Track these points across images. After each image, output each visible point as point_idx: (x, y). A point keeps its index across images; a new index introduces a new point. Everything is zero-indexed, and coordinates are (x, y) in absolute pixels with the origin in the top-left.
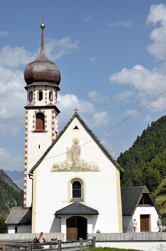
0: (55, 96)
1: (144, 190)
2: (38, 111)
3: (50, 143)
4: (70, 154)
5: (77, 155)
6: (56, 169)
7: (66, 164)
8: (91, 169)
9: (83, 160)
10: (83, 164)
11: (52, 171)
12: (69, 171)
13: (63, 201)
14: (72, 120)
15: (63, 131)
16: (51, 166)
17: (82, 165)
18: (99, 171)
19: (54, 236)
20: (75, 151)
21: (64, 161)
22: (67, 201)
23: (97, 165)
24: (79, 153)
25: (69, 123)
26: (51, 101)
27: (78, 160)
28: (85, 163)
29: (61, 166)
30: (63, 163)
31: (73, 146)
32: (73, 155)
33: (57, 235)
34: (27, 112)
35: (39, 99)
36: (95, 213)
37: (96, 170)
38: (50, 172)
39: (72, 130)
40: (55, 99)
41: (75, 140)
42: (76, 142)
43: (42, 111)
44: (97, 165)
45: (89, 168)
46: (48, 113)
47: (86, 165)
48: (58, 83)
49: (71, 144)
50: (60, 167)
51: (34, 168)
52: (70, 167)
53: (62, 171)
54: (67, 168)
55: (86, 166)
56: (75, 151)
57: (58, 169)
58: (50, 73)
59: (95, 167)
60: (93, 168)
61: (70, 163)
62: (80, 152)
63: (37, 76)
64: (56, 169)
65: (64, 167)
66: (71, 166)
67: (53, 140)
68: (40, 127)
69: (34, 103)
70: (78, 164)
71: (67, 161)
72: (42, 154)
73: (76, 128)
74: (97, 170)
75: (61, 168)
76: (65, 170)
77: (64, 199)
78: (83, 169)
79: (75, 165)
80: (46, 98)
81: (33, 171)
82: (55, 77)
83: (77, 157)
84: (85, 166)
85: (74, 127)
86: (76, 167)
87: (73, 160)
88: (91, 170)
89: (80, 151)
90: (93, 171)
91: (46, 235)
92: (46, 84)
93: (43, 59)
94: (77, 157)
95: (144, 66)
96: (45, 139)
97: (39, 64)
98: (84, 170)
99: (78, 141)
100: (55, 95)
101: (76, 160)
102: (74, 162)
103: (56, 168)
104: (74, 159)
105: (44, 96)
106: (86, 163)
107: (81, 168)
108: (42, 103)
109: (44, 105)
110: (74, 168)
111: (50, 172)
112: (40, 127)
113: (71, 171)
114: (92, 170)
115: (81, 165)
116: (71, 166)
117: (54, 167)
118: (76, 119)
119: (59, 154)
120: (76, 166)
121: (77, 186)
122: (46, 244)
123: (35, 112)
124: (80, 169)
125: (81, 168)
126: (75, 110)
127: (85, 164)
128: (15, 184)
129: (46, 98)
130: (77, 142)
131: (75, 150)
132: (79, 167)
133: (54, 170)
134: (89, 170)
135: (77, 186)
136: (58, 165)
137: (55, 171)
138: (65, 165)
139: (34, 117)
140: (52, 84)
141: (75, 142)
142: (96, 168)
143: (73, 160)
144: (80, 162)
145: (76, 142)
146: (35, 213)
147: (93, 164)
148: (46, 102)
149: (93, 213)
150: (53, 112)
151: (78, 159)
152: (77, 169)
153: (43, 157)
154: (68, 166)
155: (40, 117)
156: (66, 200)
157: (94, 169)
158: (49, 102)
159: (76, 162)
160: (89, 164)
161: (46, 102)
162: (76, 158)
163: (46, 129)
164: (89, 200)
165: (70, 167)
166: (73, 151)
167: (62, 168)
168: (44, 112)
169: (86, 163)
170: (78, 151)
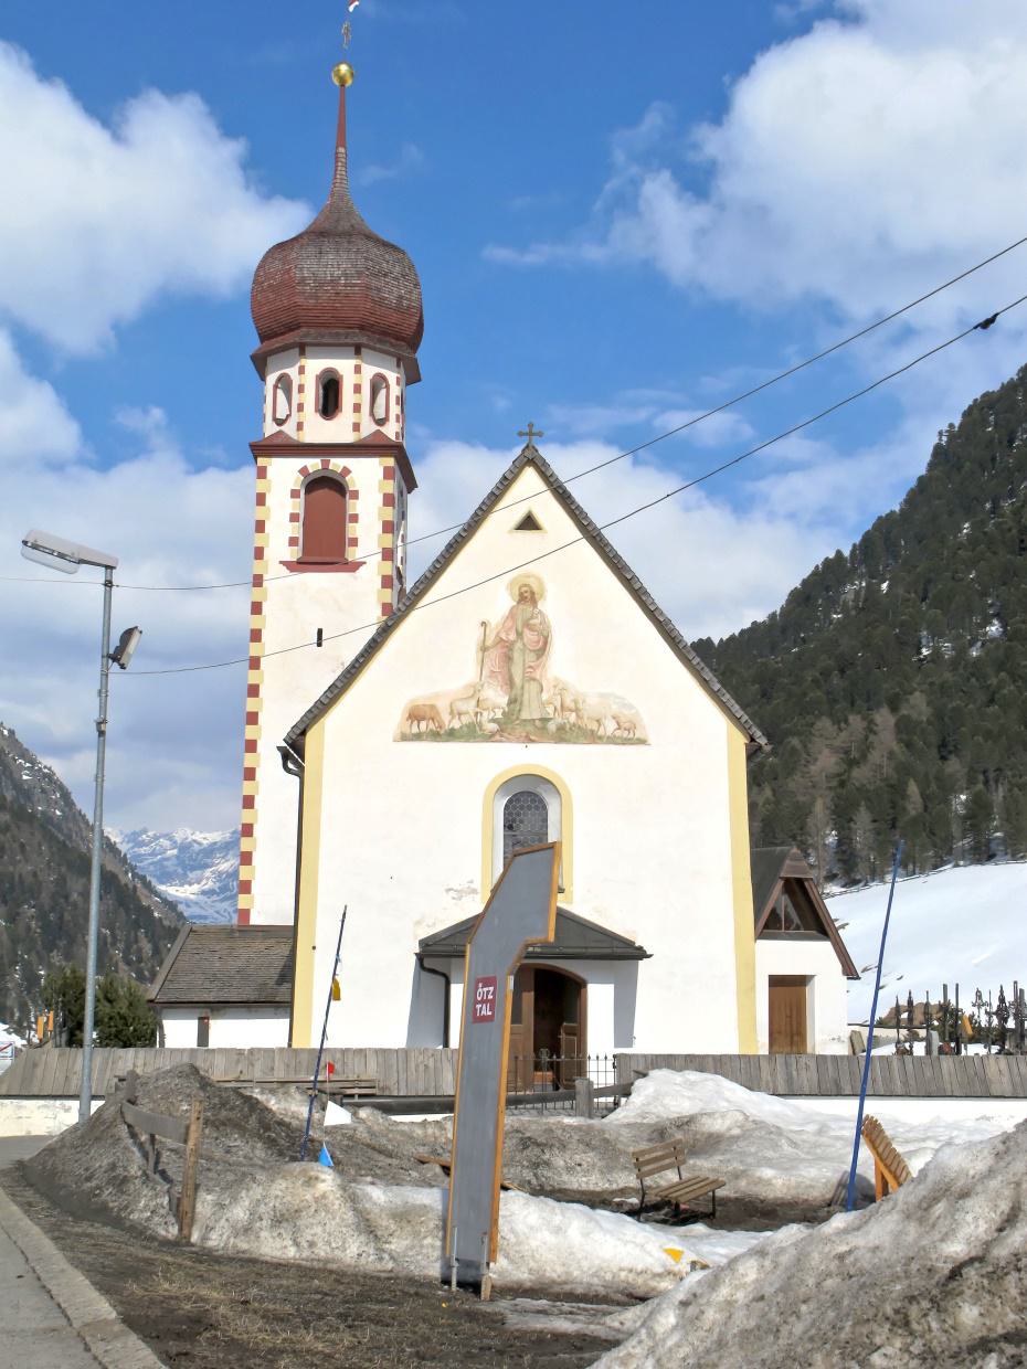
0: (397, 403)
1: (788, 862)
2: (314, 464)
3: (374, 617)
4: (494, 655)
5: (531, 657)
6: (424, 724)
7: (474, 702)
8: (601, 732)
9: (560, 686)
10: (562, 706)
11: (404, 738)
12: (490, 738)
13: (459, 888)
14: (506, 482)
15: (464, 535)
16: (395, 719)
17: (559, 707)
18: (642, 742)
19: (422, 1068)
20: (520, 641)
21: (467, 687)
22: (474, 891)
23: (633, 711)
24: (542, 650)
25: (494, 498)
26: (381, 422)
27: (533, 687)
28: (572, 698)
29: (452, 713)
30: (462, 699)
31: (512, 615)
32: (508, 659)
33: (435, 1061)
34: (262, 473)
35: (320, 407)
36: (622, 954)
37: (629, 736)
38: (391, 739)
39: (510, 532)
40: (397, 416)
41: (525, 585)
42: (528, 597)
43: (337, 463)
44: (633, 711)
45: (594, 726)
46: (367, 477)
47: (577, 710)
48: (414, 340)
49: (499, 604)
50: (446, 717)
51: (311, 716)
52: (493, 720)
53: (452, 735)
54: (480, 725)
55: (578, 716)
56: (520, 641)
57: (431, 726)
58: (379, 290)
59: (623, 719)
60: (610, 727)
61: (497, 697)
62: (546, 643)
63: (317, 298)
64: (424, 724)
65: (465, 720)
66: (499, 715)
67: (386, 608)
68: (323, 546)
69: (300, 426)
70: (535, 705)
71: (482, 686)
72: (334, 672)
73: (529, 523)
74: (631, 736)
75: (447, 723)
76: (471, 733)
77: (457, 877)
78: (561, 728)
79: (520, 710)
80: (357, 408)
81: (303, 733)
82: (398, 309)
83: (530, 667)
84: (574, 714)
85: (518, 515)
86: (525, 720)
87: (510, 683)
88: (600, 738)
89: (546, 638)
90: (612, 740)
91: (381, 1060)
92: (356, 340)
93: (344, 225)
94: (530, 667)
95: (140, 901)
96: (352, 598)
97: (327, 245)
98: (563, 735)
99: (536, 589)
100: (397, 397)
101: (526, 685)
102: (514, 692)
103: (423, 725)
104: (518, 680)
105: (348, 397)
106: (576, 702)
107: (552, 726)
108: (339, 430)
109: (349, 437)
110: (510, 726)
111: (395, 741)
112: (323, 546)
113: (498, 737)
114: (608, 737)
115: (550, 710)
116: (499, 715)
117: (415, 715)
118: (530, 476)
119: (441, 652)
120: (525, 715)
121: (526, 814)
122: (399, 1105)
123: (304, 471)
124: (544, 728)
125: (552, 726)
126: (527, 434)
127: (572, 706)
128: (143, 879)
129: (357, 408)
130: (533, 593)
131: (520, 635)
132: (541, 719)
133: (415, 730)
134: (593, 738)
135: (526, 814)
136: (433, 707)
137: (418, 737)
138: (470, 706)
139: (295, 494)
140: (386, 342)
141: (521, 594)
142: (627, 725)
143: (510, 683)
144: (545, 696)
145: (528, 597)
146: (314, 948)
147: (614, 707)
148: (356, 427)
149: (619, 950)
150: (388, 473)
151: (534, 679)
152: (530, 728)
153: (357, 665)
154: (485, 714)
155: (326, 490)
156: (472, 882)
157: (618, 733)
158: (369, 427)
159: (526, 696)
160: (592, 705)
161: (356, 427)
162: (524, 669)
163: (353, 554)
164: (592, 891)
165: (493, 720)
166: (512, 637)
167: (456, 724)
168: (346, 471)
169: (576, 702)
170: (536, 638)
